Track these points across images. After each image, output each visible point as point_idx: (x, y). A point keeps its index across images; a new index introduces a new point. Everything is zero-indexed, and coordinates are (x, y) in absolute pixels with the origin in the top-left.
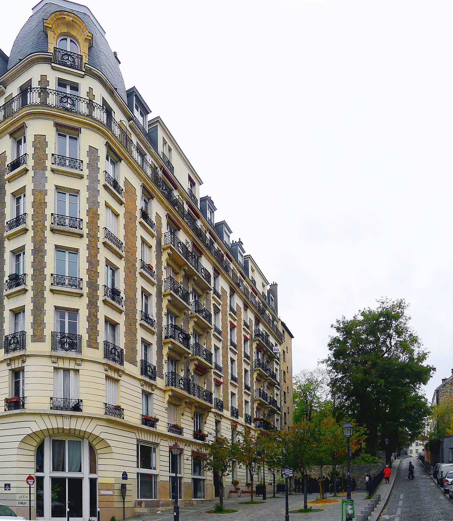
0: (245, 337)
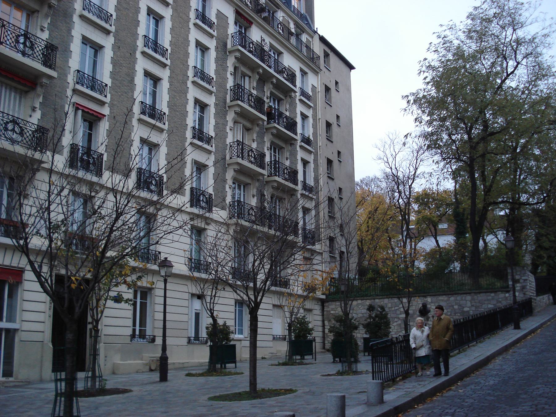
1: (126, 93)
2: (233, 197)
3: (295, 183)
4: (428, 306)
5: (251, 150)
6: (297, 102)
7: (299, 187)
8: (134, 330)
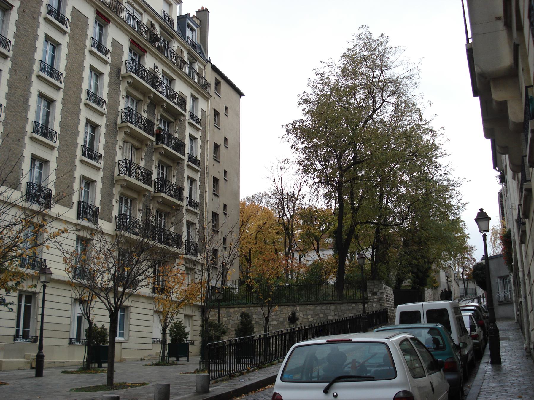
1: (20, 113)
2: (120, 211)
3: (181, 199)
4: (297, 314)
6: (187, 124)
7: (185, 203)
8: (18, 331)
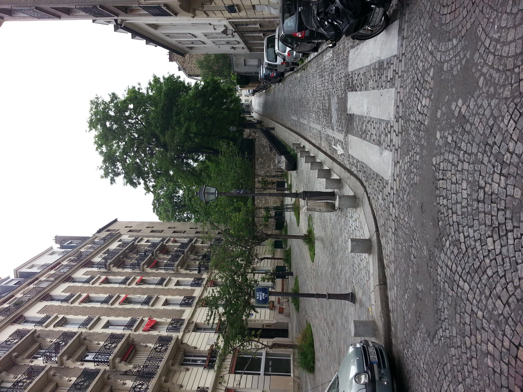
0: (103, 282)
5: (105, 346)
